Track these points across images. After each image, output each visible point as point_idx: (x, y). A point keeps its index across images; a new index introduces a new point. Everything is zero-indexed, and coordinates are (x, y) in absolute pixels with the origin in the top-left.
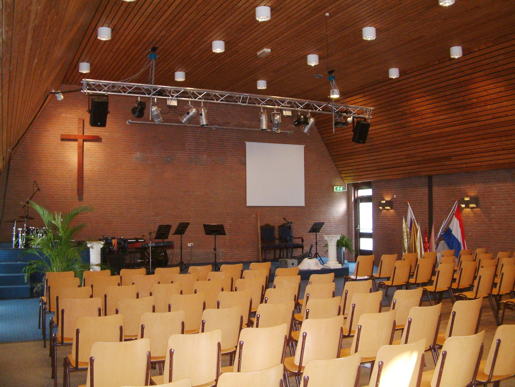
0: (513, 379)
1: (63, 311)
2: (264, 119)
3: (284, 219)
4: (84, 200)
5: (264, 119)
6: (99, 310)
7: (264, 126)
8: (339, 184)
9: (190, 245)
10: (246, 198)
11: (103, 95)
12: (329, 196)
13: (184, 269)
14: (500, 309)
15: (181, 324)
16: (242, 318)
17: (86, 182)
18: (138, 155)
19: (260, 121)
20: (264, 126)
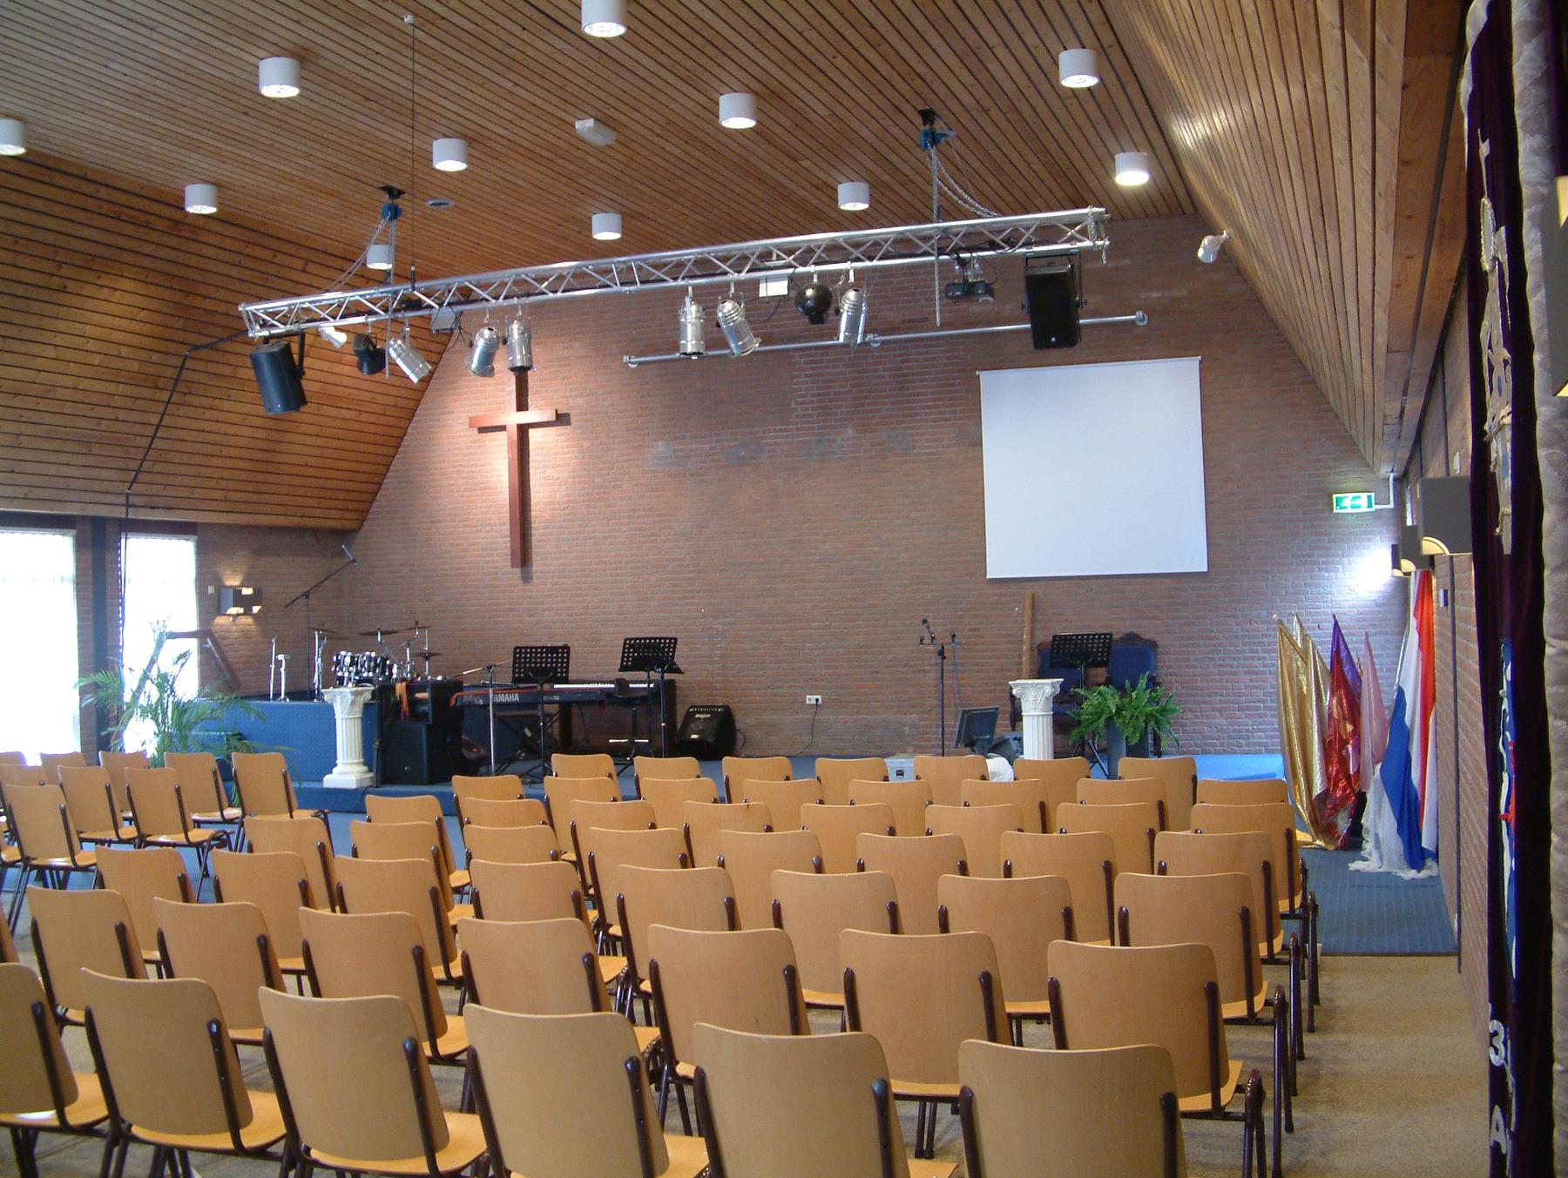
0: (1474, 1131)
1: (592, 859)
2: (691, 313)
3: (925, 621)
4: (535, 581)
5: (691, 313)
6: (304, 887)
7: (690, 343)
8: (1359, 485)
9: (811, 699)
10: (1474, 521)
11: (1066, 255)
12: (1317, 534)
13: (802, 760)
14: (63, 1021)
15: (724, 909)
16: (1267, 869)
17: (537, 533)
18: (661, 448)
19: (678, 330)
20: (690, 343)
